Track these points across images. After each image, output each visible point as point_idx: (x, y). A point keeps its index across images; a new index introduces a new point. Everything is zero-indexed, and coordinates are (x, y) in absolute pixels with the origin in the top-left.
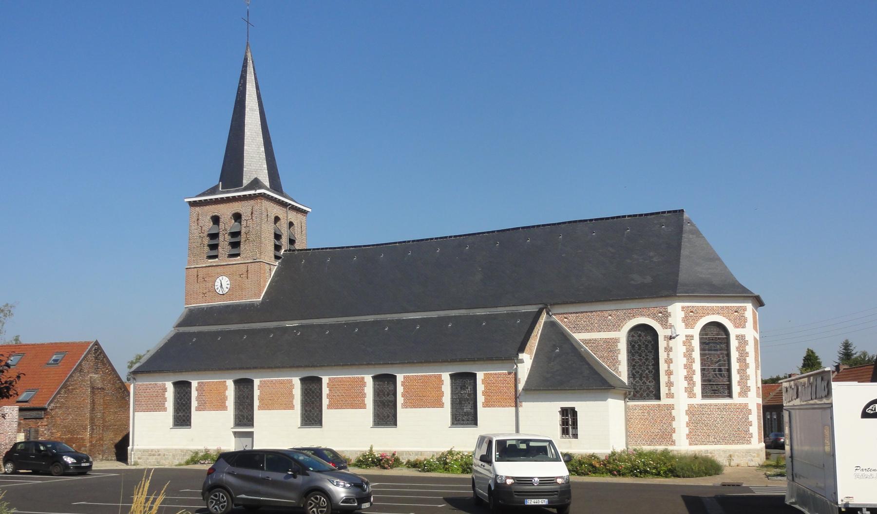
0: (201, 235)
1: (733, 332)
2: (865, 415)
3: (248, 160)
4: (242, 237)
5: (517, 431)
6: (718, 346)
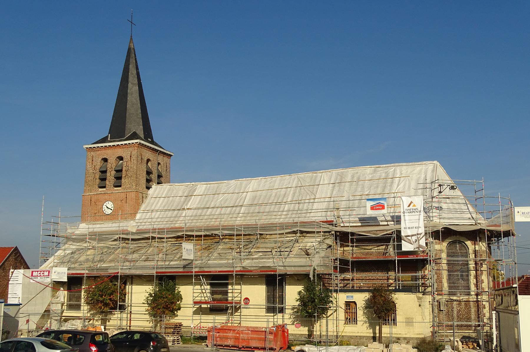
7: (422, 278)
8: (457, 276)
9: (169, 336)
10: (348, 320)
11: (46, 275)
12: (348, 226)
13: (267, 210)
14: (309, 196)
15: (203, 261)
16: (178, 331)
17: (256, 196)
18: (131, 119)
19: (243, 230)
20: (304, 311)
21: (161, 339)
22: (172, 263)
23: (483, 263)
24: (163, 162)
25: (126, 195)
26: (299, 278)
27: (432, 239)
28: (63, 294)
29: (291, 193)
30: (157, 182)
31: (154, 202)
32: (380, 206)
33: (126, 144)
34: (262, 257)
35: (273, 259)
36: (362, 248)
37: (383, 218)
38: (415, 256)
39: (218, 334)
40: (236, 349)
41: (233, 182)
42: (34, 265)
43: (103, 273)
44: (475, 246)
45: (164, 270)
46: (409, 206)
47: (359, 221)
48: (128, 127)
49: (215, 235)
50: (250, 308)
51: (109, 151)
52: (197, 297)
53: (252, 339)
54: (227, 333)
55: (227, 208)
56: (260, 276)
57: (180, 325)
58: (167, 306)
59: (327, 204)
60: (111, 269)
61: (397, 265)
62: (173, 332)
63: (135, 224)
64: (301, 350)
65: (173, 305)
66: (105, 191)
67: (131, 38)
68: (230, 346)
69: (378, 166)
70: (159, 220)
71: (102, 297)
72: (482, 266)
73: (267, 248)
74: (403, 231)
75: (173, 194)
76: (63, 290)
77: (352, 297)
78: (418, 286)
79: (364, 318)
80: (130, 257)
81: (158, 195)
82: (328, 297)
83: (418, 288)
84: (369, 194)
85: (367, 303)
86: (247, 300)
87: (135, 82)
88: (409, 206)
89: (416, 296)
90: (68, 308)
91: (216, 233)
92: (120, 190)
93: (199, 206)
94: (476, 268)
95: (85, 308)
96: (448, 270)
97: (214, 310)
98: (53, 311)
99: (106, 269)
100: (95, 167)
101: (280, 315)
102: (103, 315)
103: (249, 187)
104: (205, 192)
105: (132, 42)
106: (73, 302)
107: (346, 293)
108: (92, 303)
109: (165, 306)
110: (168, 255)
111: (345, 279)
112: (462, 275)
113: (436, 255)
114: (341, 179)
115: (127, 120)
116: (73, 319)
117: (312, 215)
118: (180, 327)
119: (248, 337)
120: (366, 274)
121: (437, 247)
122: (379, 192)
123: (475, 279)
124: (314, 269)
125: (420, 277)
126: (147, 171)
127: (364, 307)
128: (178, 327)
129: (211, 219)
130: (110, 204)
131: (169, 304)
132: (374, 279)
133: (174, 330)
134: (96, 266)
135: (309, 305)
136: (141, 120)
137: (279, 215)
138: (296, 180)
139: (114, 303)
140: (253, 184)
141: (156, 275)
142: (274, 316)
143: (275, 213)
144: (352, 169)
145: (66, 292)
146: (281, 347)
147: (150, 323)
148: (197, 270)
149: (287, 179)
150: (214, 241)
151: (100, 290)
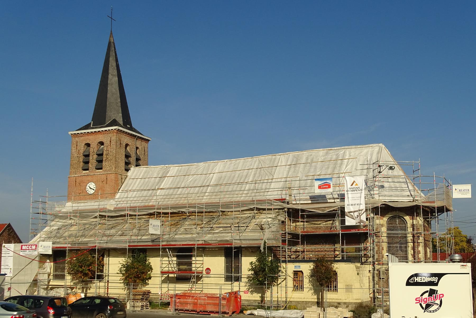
2: (408, 284)
5: (469, 274)
7: (364, 250)
8: (396, 248)
9: (138, 302)
10: (296, 287)
11: (33, 249)
12: (299, 204)
13: (230, 190)
14: (268, 176)
15: (171, 236)
16: (146, 298)
17: (221, 177)
18: (111, 107)
19: (205, 208)
20: (256, 280)
21: (118, 303)
22: (144, 238)
23: (420, 236)
24: (141, 147)
25: (107, 176)
26: (252, 250)
27: (373, 214)
28: (49, 266)
29: (252, 174)
30: (136, 165)
31: (132, 183)
32: (326, 185)
33: (106, 130)
34: (222, 232)
35: (231, 233)
36: (312, 223)
37: (331, 196)
38: (357, 230)
39: (178, 300)
40: (195, 313)
41: (202, 164)
43: (82, 247)
44: (413, 221)
45: (136, 244)
46: (352, 185)
47: (309, 199)
48: (108, 115)
49: (181, 212)
50: (211, 277)
51: (91, 137)
52: (166, 267)
53: (208, 304)
54: (187, 299)
55: (195, 188)
56: (220, 249)
57: (148, 293)
58: (138, 275)
59: (283, 184)
60: (90, 243)
61: (340, 238)
62: (141, 298)
63: (114, 203)
64: (251, 314)
65: (144, 274)
66: (88, 173)
67: (111, 33)
68: (190, 310)
69: (330, 149)
70: (135, 199)
71: (81, 267)
72: (419, 238)
73: (227, 224)
74: (347, 207)
75: (149, 175)
76: (49, 262)
77: (299, 266)
78: (361, 257)
79: (309, 286)
80: (108, 232)
81: (136, 176)
82: (278, 267)
83: (361, 258)
84: (320, 174)
85: (312, 272)
86: (209, 270)
87: (115, 74)
88: (352, 185)
89: (355, 265)
90: (54, 278)
91: (183, 211)
92: (101, 172)
93: (171, 186)
94: (414, 240)
95: (68, 277)
96: (388, 242)
97: (181, 279)
98: (40, 281)
99: (86, 243)
100: (79, 151)
101: (236, 284)
102: (84, 284)
103: (216, 169)
104: (177, 174)
105: (112, 36)
106: (59, 272)
107: (294, 263)
108: (75, 273)
109: (136, 275)
110: (141, 231)
111: (297, 251)
112: (401, 247)
113: (377, 229)
114: (297, 161)
115: (108, 109)
116: (58, 288)
117: (269, 193)
118: (149, 294)
119: (205, 303)
120: (315, 246)
121: (378, 222)
122: (329, 172)
123: (412, 250)
124: (265, 242)
125: (363, 249)
126: (125, 155)
127: (309, 276)
128: (147, 294)
129: (138, 200)
130: (92, 185)
131: (139, 274)
132: (322, 251)
133: (142, 297)
134: (78, 241)
135: (260, 274)
136: (120, 108)
137: (240, 194)
138: (257, 162)
139: (93, 273)
140: (219, 166)
141: (128, 248)
142: (231, 284)
143: (237, 192)
144: (307, 152)
145: (52, 264)
146: (234, 311)
147: (124, 291)
148: (164, 243)
149: (249, 161)
150: (182, 218)
151: (80, 262)
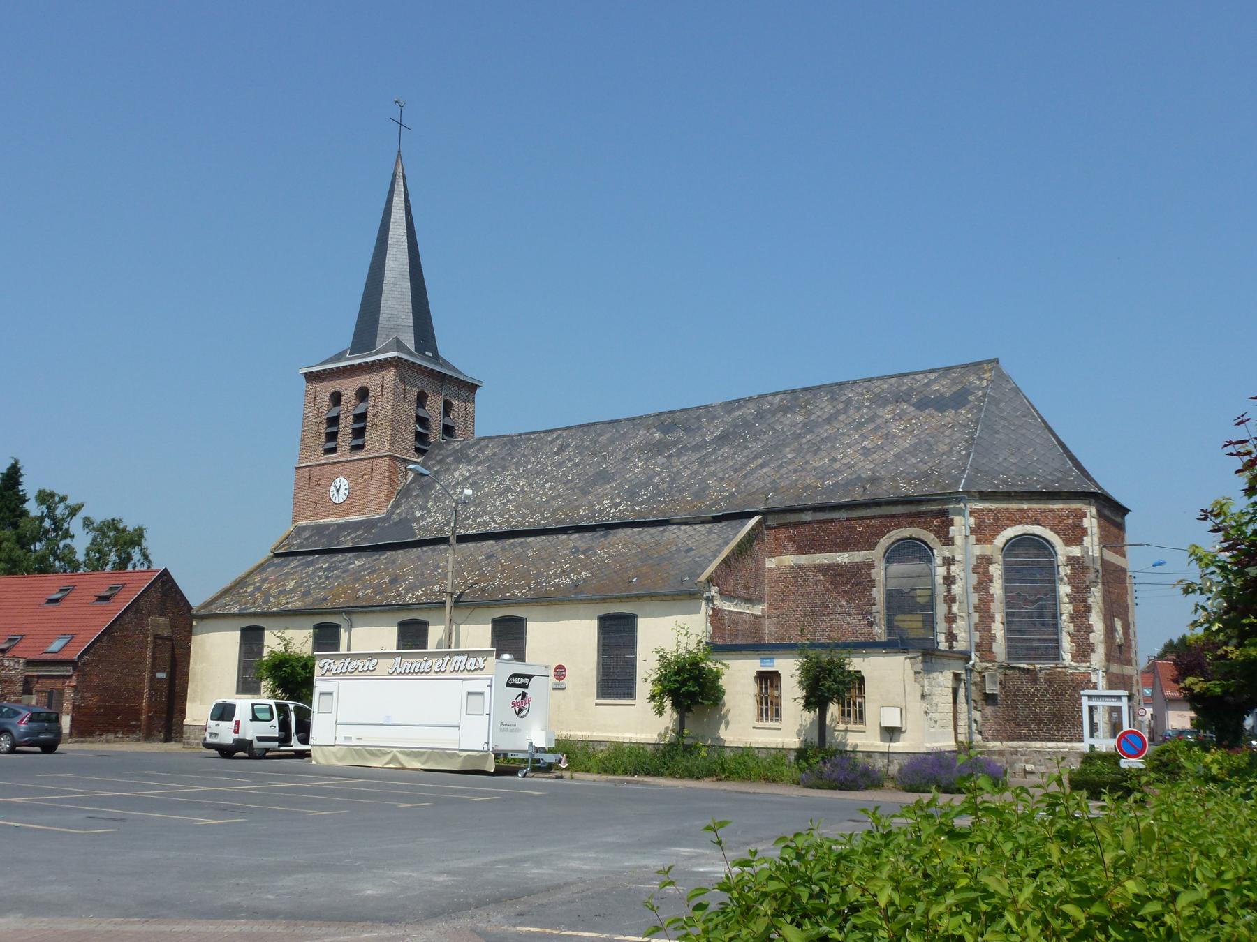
0: (317, 419)
1: (1063, 552)
2: (508, 685)
3: (387, 312)
4: (368, 420)
6: (1038, 575)
42: (926, 712)
130: (343, 483)
